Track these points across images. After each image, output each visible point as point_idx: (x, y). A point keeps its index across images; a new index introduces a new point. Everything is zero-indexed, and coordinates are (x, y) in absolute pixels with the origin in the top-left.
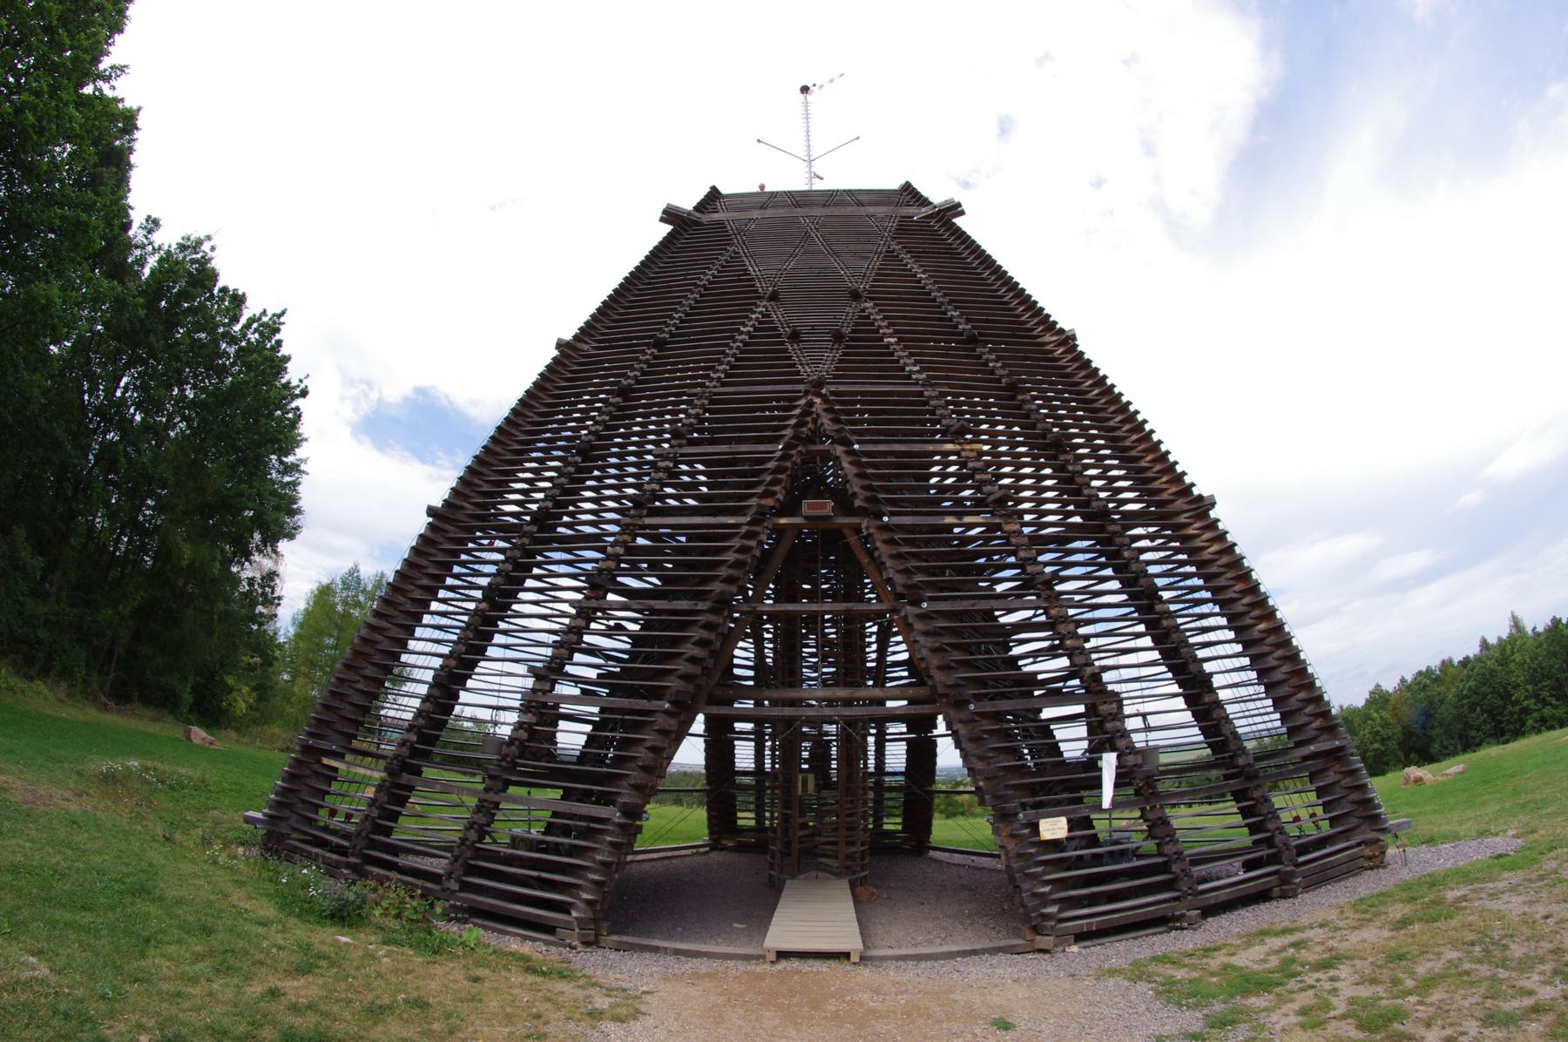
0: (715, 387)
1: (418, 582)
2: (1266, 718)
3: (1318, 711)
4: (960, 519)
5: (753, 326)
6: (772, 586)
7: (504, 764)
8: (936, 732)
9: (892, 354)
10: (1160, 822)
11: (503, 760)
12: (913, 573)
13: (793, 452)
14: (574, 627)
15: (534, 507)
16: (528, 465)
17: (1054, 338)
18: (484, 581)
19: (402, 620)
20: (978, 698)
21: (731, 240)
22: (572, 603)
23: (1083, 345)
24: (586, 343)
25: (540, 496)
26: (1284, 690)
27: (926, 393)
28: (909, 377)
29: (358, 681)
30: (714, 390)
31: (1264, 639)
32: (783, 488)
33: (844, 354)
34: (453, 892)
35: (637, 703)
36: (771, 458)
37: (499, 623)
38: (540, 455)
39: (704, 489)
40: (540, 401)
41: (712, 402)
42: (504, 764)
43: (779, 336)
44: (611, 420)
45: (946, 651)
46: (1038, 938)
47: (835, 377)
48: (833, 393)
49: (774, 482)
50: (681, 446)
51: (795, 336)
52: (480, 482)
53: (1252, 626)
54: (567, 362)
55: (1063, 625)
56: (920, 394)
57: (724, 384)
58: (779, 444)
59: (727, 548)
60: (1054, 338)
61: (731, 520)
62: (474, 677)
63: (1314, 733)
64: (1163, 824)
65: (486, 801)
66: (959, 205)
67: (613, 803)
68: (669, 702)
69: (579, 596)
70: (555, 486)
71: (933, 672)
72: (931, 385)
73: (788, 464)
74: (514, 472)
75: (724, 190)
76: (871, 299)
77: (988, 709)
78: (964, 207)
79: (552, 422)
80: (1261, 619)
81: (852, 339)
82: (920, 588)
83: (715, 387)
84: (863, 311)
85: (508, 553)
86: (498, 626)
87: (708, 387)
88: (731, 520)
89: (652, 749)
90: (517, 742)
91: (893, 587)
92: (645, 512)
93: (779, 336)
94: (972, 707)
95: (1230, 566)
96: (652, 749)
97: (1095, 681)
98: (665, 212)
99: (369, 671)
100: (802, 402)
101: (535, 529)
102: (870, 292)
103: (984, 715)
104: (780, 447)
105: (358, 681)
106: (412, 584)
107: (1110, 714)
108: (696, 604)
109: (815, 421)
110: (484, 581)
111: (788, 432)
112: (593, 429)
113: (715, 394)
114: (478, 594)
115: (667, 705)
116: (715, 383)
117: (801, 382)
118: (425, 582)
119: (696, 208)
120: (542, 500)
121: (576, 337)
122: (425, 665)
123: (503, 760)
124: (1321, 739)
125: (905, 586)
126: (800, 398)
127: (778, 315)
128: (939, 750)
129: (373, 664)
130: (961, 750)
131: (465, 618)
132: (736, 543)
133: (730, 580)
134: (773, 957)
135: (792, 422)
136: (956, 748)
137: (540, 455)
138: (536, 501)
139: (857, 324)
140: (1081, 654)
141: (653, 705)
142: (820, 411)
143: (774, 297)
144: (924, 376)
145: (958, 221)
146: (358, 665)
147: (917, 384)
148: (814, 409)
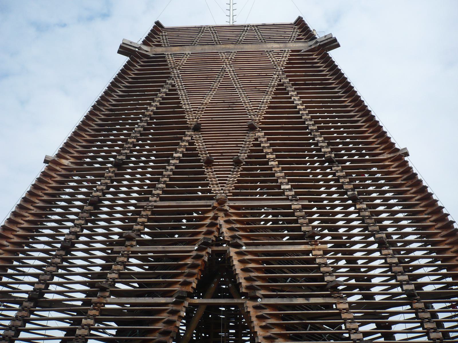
0: (155, 201)
5: (182, 152)
6: (195, 338)
13: (204, 253)
15: (62, 238)
16: (63, 197)
21: (169, 73)
24: (67, 159)
25: (66, 231)
27: (293, 207)
28: (282, 194)
30: (155, 204)
32: (196, 279)
33: (242, 175)
36: (188, 257)
38: (71, 191)
39: (200, 194)
40: (19, 226)
41: (153, 213)
44: (144, 130)
47: (235, 194)
48: (231, 207)
49: (190, 275)
51: (209, 163)
52: (22, 222)
56: (289, 207)
57: (162, 199)
58: (195, 245)
61: (162, 300)
66: (335, 40)
70: (76, 225)
72: (297, 200)
73: (199, 262)
74: (50, 208)
75: (166, 24)
76: (263, 129)
79: (94, 146)
81: (247, 163)
83: (155, 201)
84: (256, 139)
85: (36, 286)
87: (151, 201)
88: (162, 300)
93: (199, 161)
98: (121, 47)
100: (211, 214)
101: (32, 305)
102: (263, 123)
104: (196, 248)
109: (219, 230)
111: (201, 237)
112: (73, 230)
113: (156, 207)
116: (155, 198)
117: (211, 198)
119: (145, 43)
120: (67, 234)
121: (58, 156)
126: (209, 211)
127: (199, 145)
132: (165, 316)
135: (204, 229)
137: (71, 191)
138: (63, 235)
139: (252, 151)
143: (197, 128)
144: (293, 193)
145: (333, 54)
147: (287, 199)
148: (218, 222)
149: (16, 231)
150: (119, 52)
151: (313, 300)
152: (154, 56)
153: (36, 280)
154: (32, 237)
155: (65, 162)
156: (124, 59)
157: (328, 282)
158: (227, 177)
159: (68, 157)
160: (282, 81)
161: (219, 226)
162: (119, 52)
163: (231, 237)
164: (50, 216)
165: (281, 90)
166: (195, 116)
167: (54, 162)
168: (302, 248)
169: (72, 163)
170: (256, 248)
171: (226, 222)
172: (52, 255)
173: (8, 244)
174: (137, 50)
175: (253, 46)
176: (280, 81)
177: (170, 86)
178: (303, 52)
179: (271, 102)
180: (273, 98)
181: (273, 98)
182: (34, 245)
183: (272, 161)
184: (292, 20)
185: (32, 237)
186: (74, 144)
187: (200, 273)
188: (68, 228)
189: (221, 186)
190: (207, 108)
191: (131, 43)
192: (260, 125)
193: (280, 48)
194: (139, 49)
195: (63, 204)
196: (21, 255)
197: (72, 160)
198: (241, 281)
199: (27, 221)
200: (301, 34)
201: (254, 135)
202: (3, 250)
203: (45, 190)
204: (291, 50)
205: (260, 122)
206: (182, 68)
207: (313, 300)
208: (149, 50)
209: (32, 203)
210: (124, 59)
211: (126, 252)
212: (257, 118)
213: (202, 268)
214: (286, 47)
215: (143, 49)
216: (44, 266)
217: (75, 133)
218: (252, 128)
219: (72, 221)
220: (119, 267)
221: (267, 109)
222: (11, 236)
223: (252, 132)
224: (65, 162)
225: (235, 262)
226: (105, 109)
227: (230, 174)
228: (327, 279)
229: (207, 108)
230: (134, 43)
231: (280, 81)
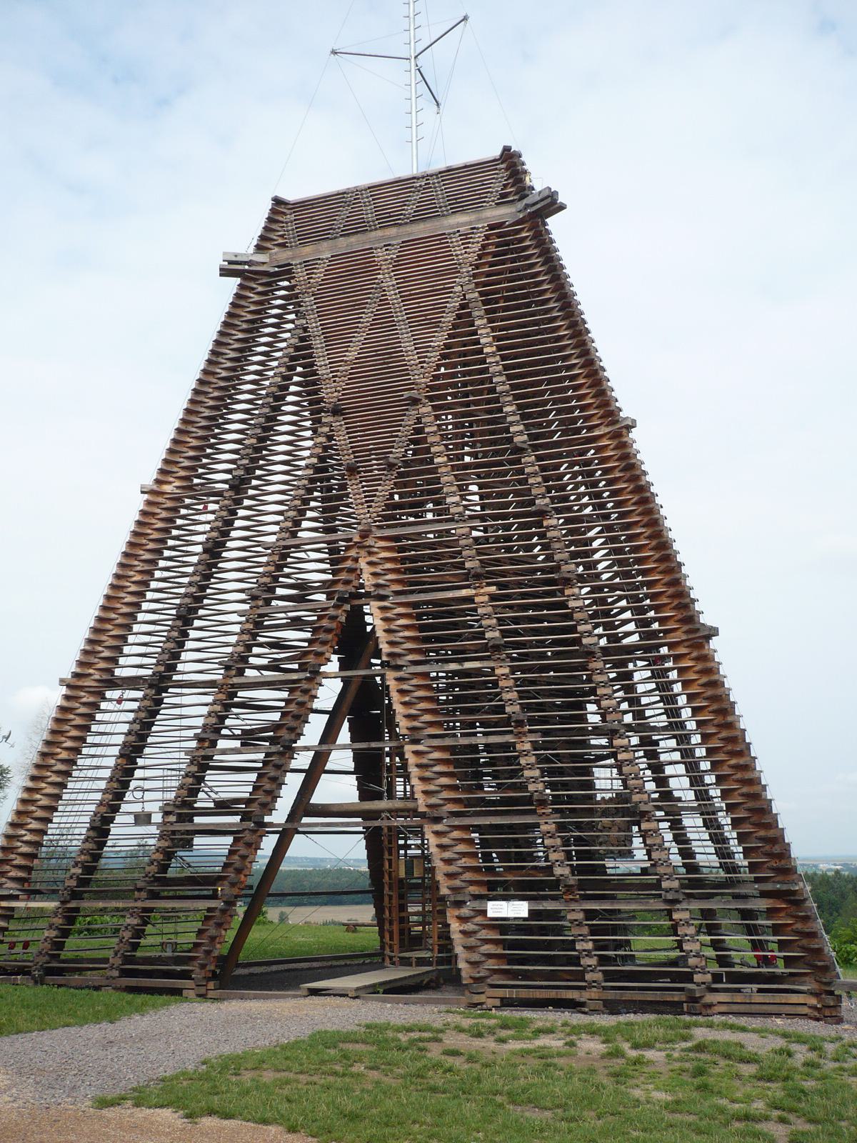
7: (147, 879)
11: (147, 876)
18: (201, 538)
22: (241, 613)
24: (170, 483)
29: (26, 835)
37: (138, 760)
40: (225, 357)
42: (147, 879)
50: (258, 607)
62: (156, 723)
69: (246, 607)
74: (268, 301)
78: (561, 199)
86: (137, 764)
90: (155, 864)
92: (234, 672)
99: (34, 825)
101: (153, 692)
105: (26, 835)
110: (201, 538)
114: (190, 570)
119: (259, 248)
120: (285, 348)
122: (116, 720)
123: (147, 876)
129: (36, 819)
131: (174, 612)
143: (336, 412)
146: (9, 858)
148: (358, 565)
149: (123, 598)
150: (221, 275)
151: (468, 665)
152: (276, 269)
153: (229, 476)
154: (234, 387)
155: (167, 488)
156: (234, 282)
157: (490, 639)
158: (377, 490)
159: (171, 479)
160: (467, 297)
161: (359, 572)
162: (221, 275)
163: (374, 585)
164: (250, 358)
165: (464, 317)
166: (336, 387)
167: (151, 492)
168: (464, 593)
169: (177, 487)
170: (406, 598)
171: (370, 563)
172: (257, 404)
173: (116, 616)
174: (247, 267)
175: (428, 225)
176: (465, 299)
177: (301, 331)
178: (509, 226)
179: (447, 346)
180: (451, 336)
181: (451, 336)
182: (229, 416)
183: (439, 456)
184: (496, 152)
185: (234, 387)
186: (243, 303)
187: (334, 643)
188: (285, 340)
189: (465, 248)
190: (352, 369)
191: (236, 256)
192: (428, 392)
193: (471, 223)
194: (249, 266)
195: (283, 293)
196: (212, 441)
197: (178, 483)
199: (212, 398)
200: (508, 184)
201: (416, 412)
202: (80, 703)
203: (230, 344)
204: (488, 225)
205: (427, 387)
206: (318, 290)
207: (468, 665)
208: (267, 260)
209: (135, 556)
210: (234, 282)
212: (423, 380)
213: (338, 631)
214: (479, 220)
215: (257, 263)
216: (244, 439)
217: (226, 324)
218: (415, 402)
219: (292, 321)
220: (326, 429)
221: (483, 240)
222: (219, 371)
223: (413, 408)
224: (167, 488)
226: (213, 388)
227: (380, 485)
228: (488, 635)
229: (352, 369)
230: (242, 255)
231: (465, 299)
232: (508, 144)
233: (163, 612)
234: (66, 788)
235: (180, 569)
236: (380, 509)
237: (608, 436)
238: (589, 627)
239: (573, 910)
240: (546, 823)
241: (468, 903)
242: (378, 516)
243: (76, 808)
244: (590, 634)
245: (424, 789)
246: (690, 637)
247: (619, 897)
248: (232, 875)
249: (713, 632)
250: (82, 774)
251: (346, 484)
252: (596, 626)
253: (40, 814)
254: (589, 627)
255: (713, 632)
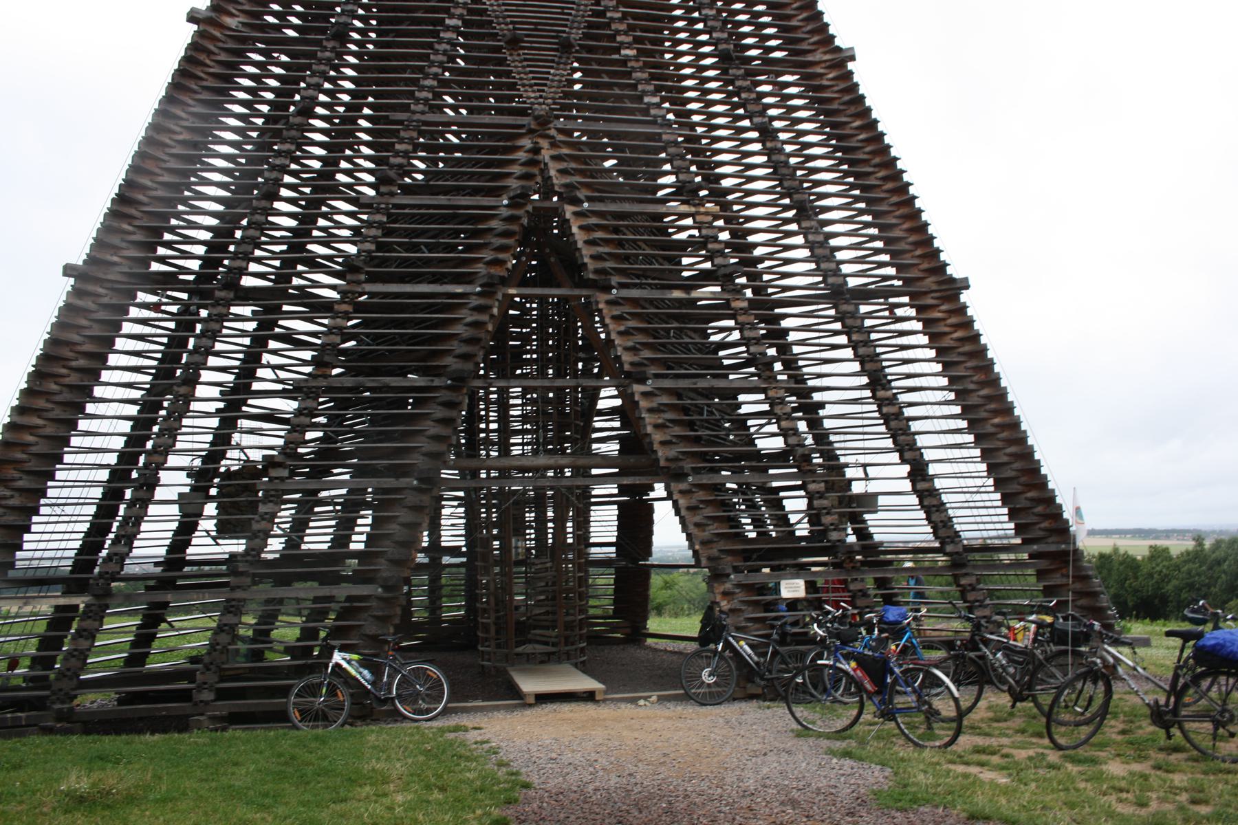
0: (423, 113)
1: (74, 364)
2: (992, 511)
3: (1048, 511)
4: (688, 293)
8: (652, 495)
9: (628, 75)
10: (860, 594)
12: (639, 350)
14: (305, 409)
17: (827, 57)
19: (58, 413)
20: (696, 471)
23: (859, 70)
26: (1014, 488)
27: (665, 137)
30: (423, 118)
31: (996, 434)
34: (207, 703)
35: (385, 482)
42: (249, 558)
43: (494, 36)
45: (668, 427)
46: (749, 685)
53: (985, 420)
54: (212, 48)
55: (780, 406)
59: (509, 175)
60: (827, 57)
61: (459, 289)
63: (1041, 534)
64: (863, 596)
65: (234, 600)
67: (528, 115)
68: (382, 586)
71: (656, 447)
77: (704, 481)
80: (996, 413)
82: (646, 365)
83: (423, 113)
87: (414, 112)
88: (459, 289)
89: (405, 525)
91: (621, 365)
94: (690, 479)
95: (971, 355)
96: (405, 525)
97: (805, 461)
103: (702, 487)
106: (64, 367)
107: (818, 492)
108: (432, 381)
115: (415, 482)
118: (82, 363)
122: (110, 431)
124: (1050, 540)
125: (632, 364)
128: (656, 517)
129: (29, 473)
130: (680, 518)
133: (465, 357)
134: (532, 700)
136: (676, 515)
139: (591, 25)
140: (794, 434)
141: (404, 482)
142: (547, 159)
148: (540, 158)
150: (966, 279)
162: (966, 279)
171: (553, 158)
198: (586, 260)
211: (383, 206)
225: (575, 230)
227: (552, 67)
232: (185, 17)
233: (155, 339)
234: (54, 480)
235: (154, 331)
236: (557, 96)
237: (823, 65)
238: (656, 100)
239: (856, 579)
240: (814, 482)
241: (732, 577)
242: (555, 103)
243: (69, 510)
244: (658, 106)
245: (663, 439)
246: (944, 287)
247: (783, 391)
248: (391, 549)
249: (964, 284)
250: (73, 475)
251: (506, 59)
252: (663, 100)
253: (33, 465)
254: (656, 100)
255: (964, 284)
